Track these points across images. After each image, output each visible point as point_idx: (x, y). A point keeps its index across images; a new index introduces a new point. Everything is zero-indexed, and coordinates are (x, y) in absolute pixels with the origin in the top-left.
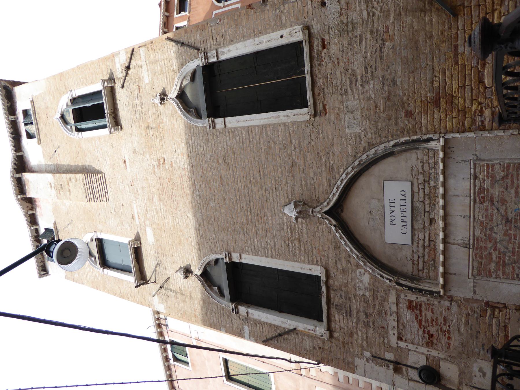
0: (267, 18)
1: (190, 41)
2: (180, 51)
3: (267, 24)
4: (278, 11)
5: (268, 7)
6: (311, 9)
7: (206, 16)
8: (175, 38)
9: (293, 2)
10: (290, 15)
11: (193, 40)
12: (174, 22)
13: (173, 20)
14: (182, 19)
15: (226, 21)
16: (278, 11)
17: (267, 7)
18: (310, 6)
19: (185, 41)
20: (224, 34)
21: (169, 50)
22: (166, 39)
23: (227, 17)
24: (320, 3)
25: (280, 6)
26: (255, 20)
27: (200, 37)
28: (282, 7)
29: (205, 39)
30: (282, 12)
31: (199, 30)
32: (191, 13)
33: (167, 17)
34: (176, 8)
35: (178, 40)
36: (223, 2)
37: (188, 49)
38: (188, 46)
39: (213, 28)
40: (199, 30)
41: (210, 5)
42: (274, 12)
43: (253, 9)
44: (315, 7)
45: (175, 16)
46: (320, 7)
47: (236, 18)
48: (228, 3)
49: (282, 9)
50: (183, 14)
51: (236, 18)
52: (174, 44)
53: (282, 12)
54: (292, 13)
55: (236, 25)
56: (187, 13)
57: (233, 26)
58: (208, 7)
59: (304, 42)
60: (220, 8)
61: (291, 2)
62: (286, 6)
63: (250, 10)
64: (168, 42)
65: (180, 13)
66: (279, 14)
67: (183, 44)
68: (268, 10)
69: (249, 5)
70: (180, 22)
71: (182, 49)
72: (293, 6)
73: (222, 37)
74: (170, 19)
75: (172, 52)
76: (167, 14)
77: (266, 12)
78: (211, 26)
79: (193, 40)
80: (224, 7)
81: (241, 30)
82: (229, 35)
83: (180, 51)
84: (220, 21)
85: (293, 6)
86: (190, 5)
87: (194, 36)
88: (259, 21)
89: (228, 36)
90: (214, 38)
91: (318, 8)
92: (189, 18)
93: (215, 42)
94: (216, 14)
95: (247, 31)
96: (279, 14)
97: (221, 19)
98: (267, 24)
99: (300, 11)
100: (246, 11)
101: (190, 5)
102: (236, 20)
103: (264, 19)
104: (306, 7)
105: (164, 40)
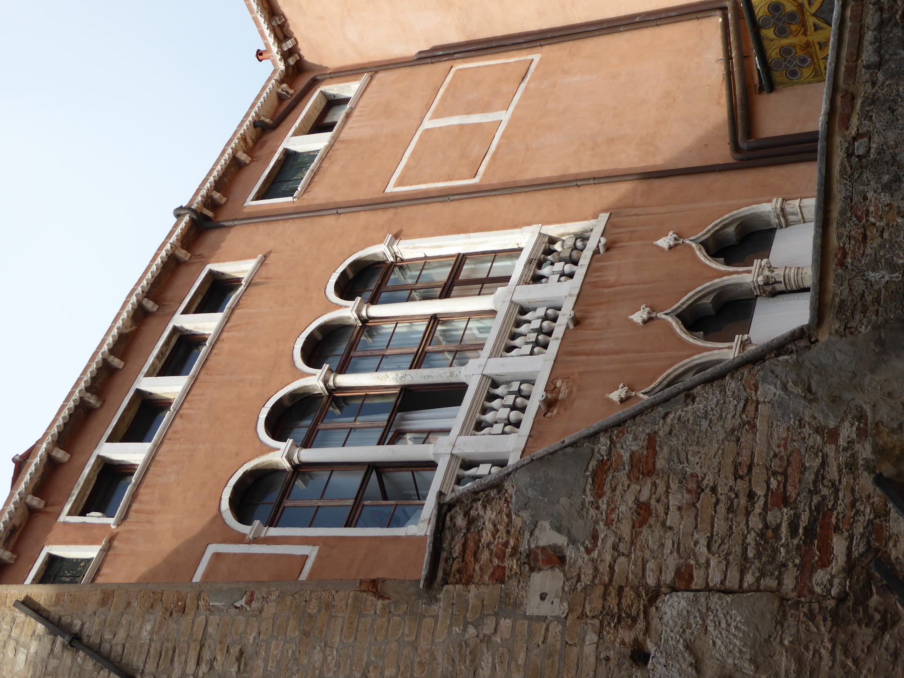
0: (424, 644)
1: (108, 636)
2: (53, 663)
3: (421, 664)
4: (471, 630)
5: (438, 608)
6: (592, 659)
7: (176, 552)
8: (55, 611)
9: (531, 618)
10: (513, 658)
11: (121, 635)
12: (51, 536)
13: (49, 529)
14: (86, 535)
15: (270, 609)
16: (471, 630)
17: (435, 607)
18: (589, 650)
19: (91, 629)
20: (249, 650)
21: (12, 644)
22: (17, 604)
23: (281, 597)
24: (628, 652)
25: (483, 616)
26: (380, 638)
27: (152, 633)
28: (490, 623)
29: (170, 645)
30: (487, 640)
31: (159, 609)
32: (121, 528)
33: (31, 512)
34: (76, 492)
35: (66, 620)
36: (257, 523)
37: (90, 664)
38: (99, 654)
39: (214, 619)
40: (159, 609)
41: (207, 519)
42: (456, 629)
43: (382, 597)
44: (608, 659)
45: (64, 517)
46: (627, 663)
47: (312, 609)
48: (274, 532)
49: (488, 630)
50: (94, 518)
51: (312, 609)
52: (40, 628)
53: (487, 640)
54: (522, 655)
55: (306, 634)
56: (111, 521)
57: (294, 633)
58: (196, 524)
59: (145, 369)
60: (241, 539)
61: (525, 617)
62: (506, 623)
63: (371, 597)
64: (21, 616)
65: (83, 513)
66: (472, 642)
67: (76, 641)
68: (436, 617)
69: (374, 582)
70: (75, 543)
71: (68, 657)
72: (531, 634)
73: (239, 659)
74: (40, 521)
75: (21, 657)
76: (35, 502)
77: (428, 622)
78: (210, 610)
79: (121, 635)
80: (256, 540)
81: (317, 656)
82: (266, 661)
83: (53, 663)
84: (249, 602)
85: (531, 634)
86: (134, 496)
87: (130, 623)
88: (394, 646)
89: (260, 662)
90: (207, 655)
91: (619, 666)
92: (111, 540)
93: (204, 668)
94: (217, 556)
95: (338, 665)
96: (472, 642)
97: (257, 595)
98: (421, 664)
99: (551, 655)
100: (356, 598)
101: (134, 496)
102: (310, 616)
103: (414, 646)
104: (575, 650)
105: (10, 602)
